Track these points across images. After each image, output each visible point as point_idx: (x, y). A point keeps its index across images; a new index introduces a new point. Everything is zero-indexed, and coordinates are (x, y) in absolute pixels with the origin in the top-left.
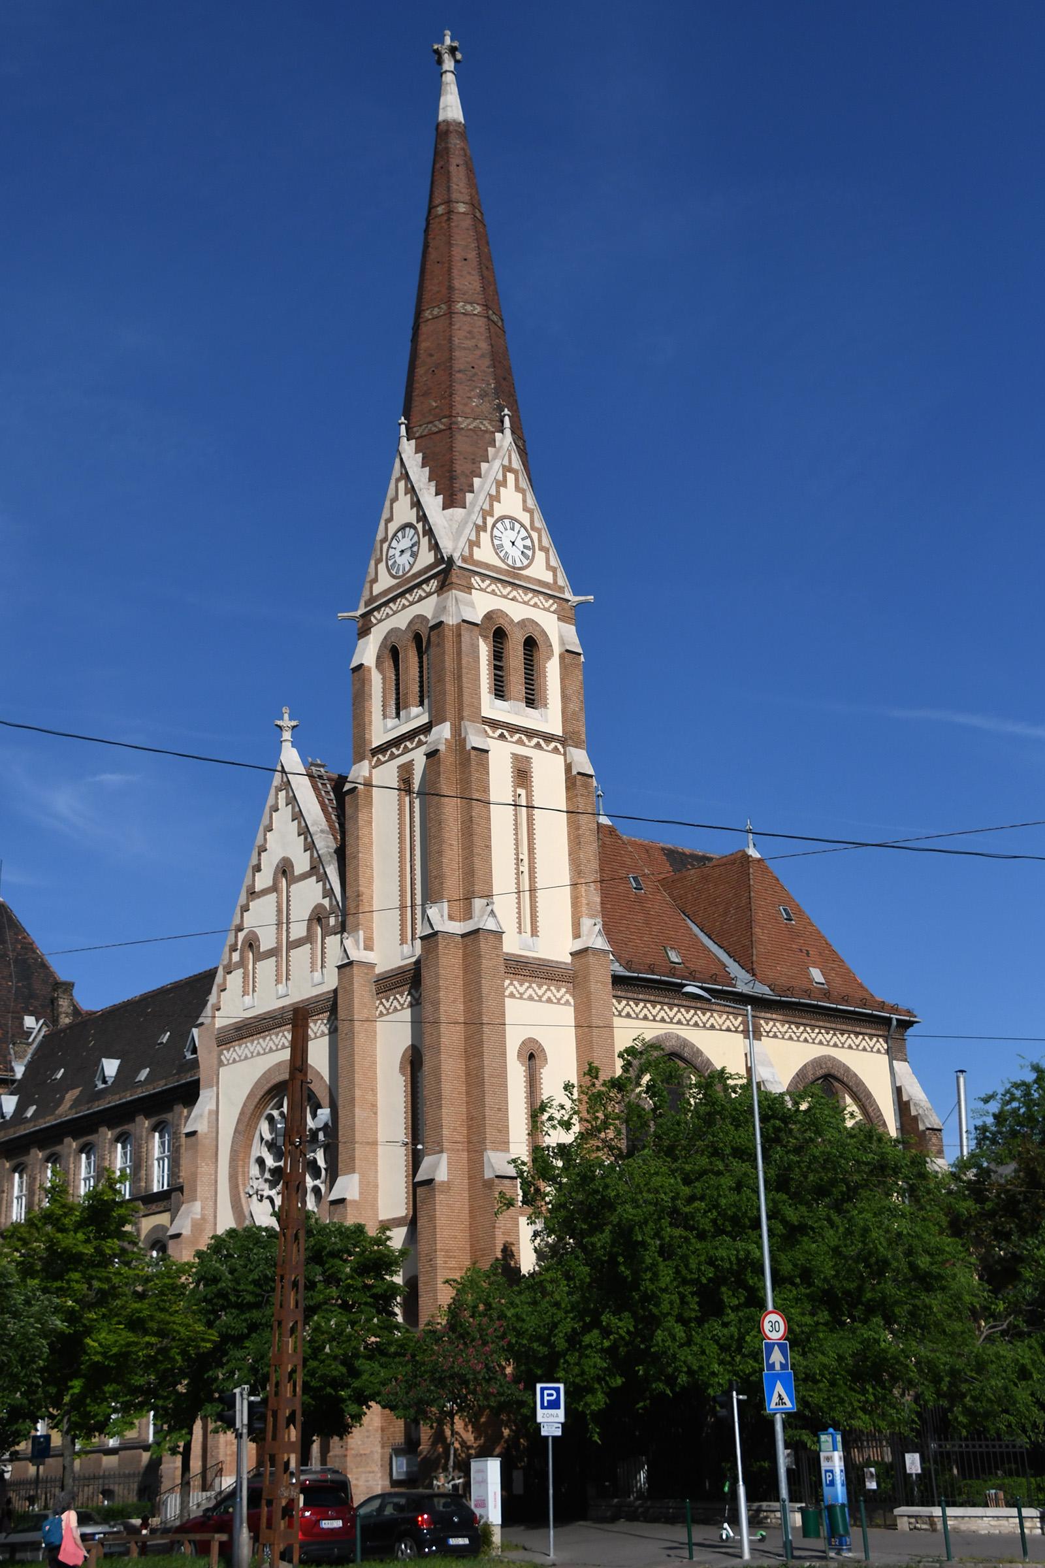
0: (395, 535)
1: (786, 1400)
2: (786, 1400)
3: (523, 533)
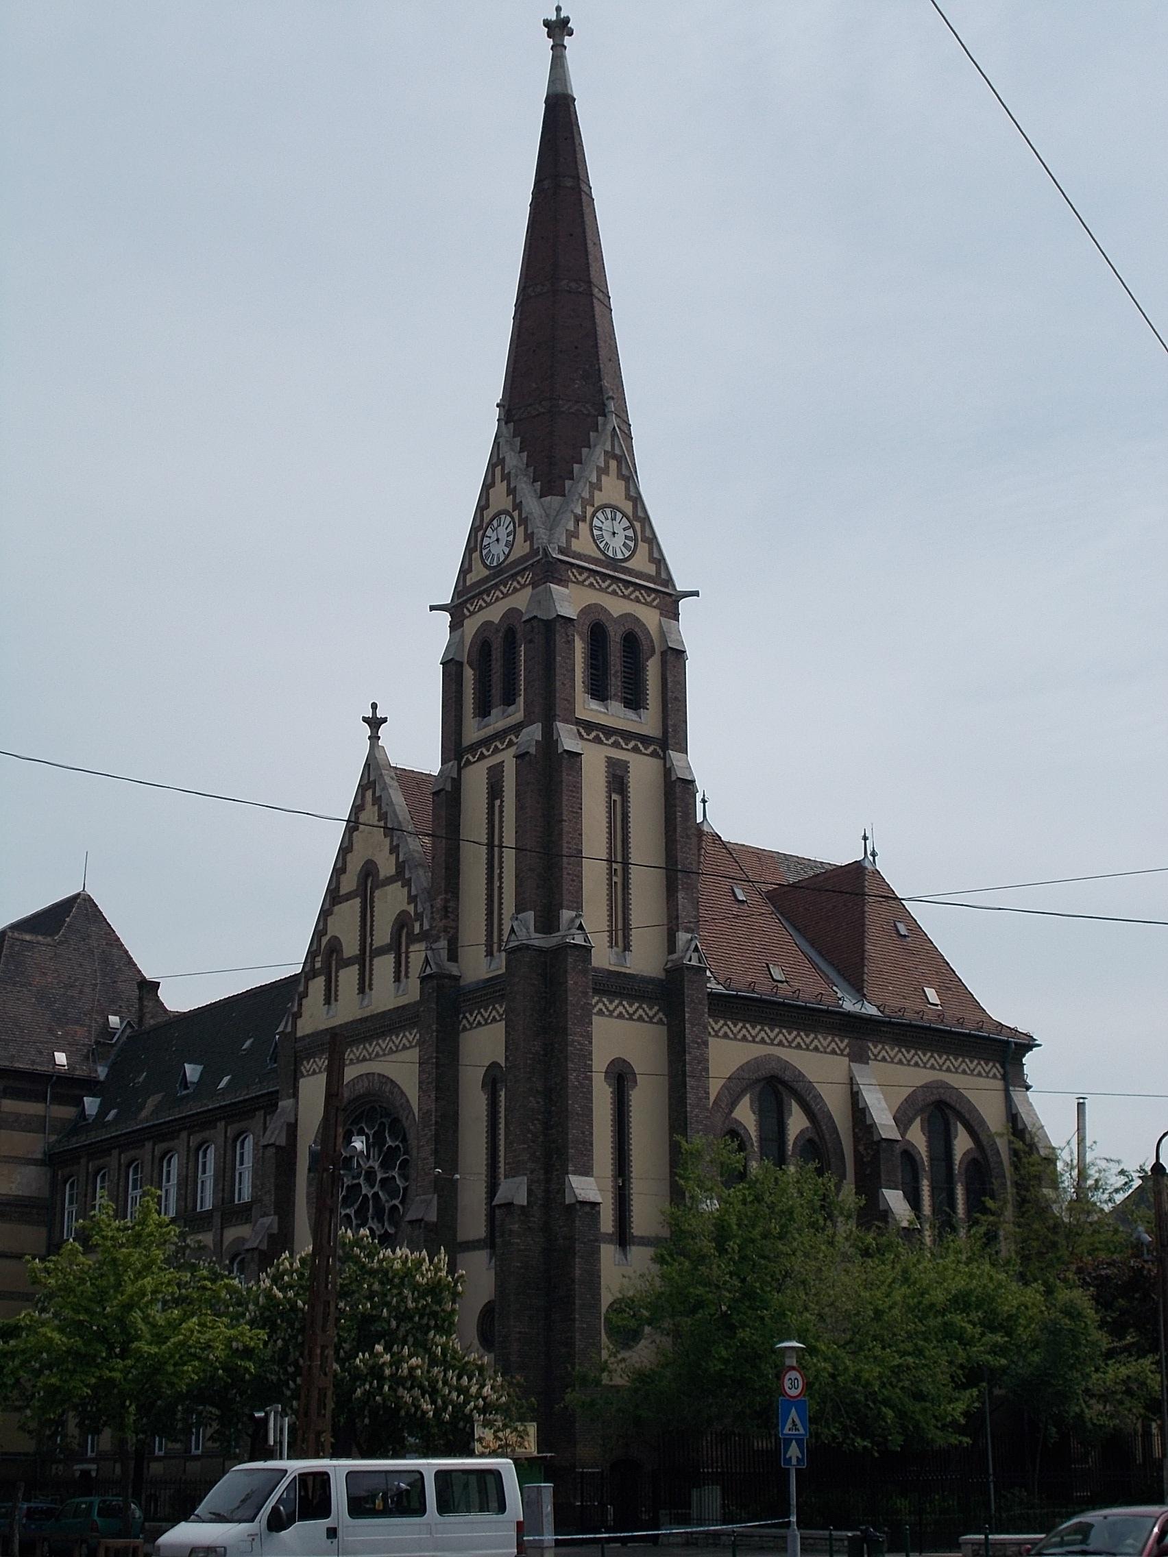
1: (799, 1426)
2: (799, 1426)
3: (626, 523)
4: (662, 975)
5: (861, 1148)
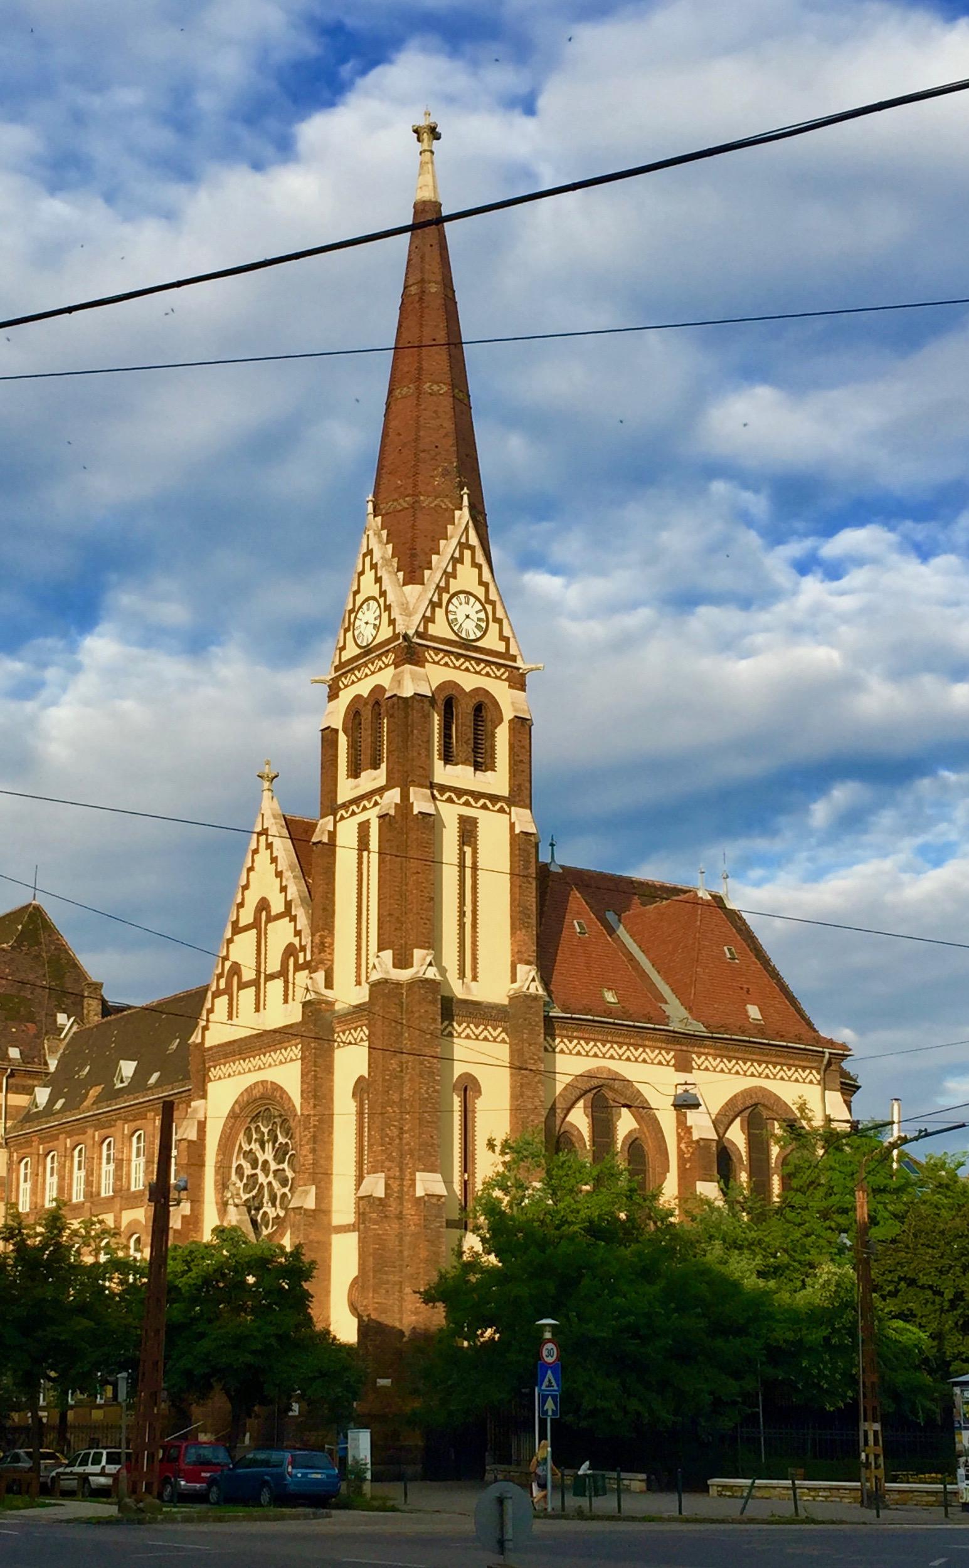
0: (360, 607)
1: (554, 1383)
2: (554, 1383)
3: (478, 606)
4: (506, 1002)
5: (683, 1146)
